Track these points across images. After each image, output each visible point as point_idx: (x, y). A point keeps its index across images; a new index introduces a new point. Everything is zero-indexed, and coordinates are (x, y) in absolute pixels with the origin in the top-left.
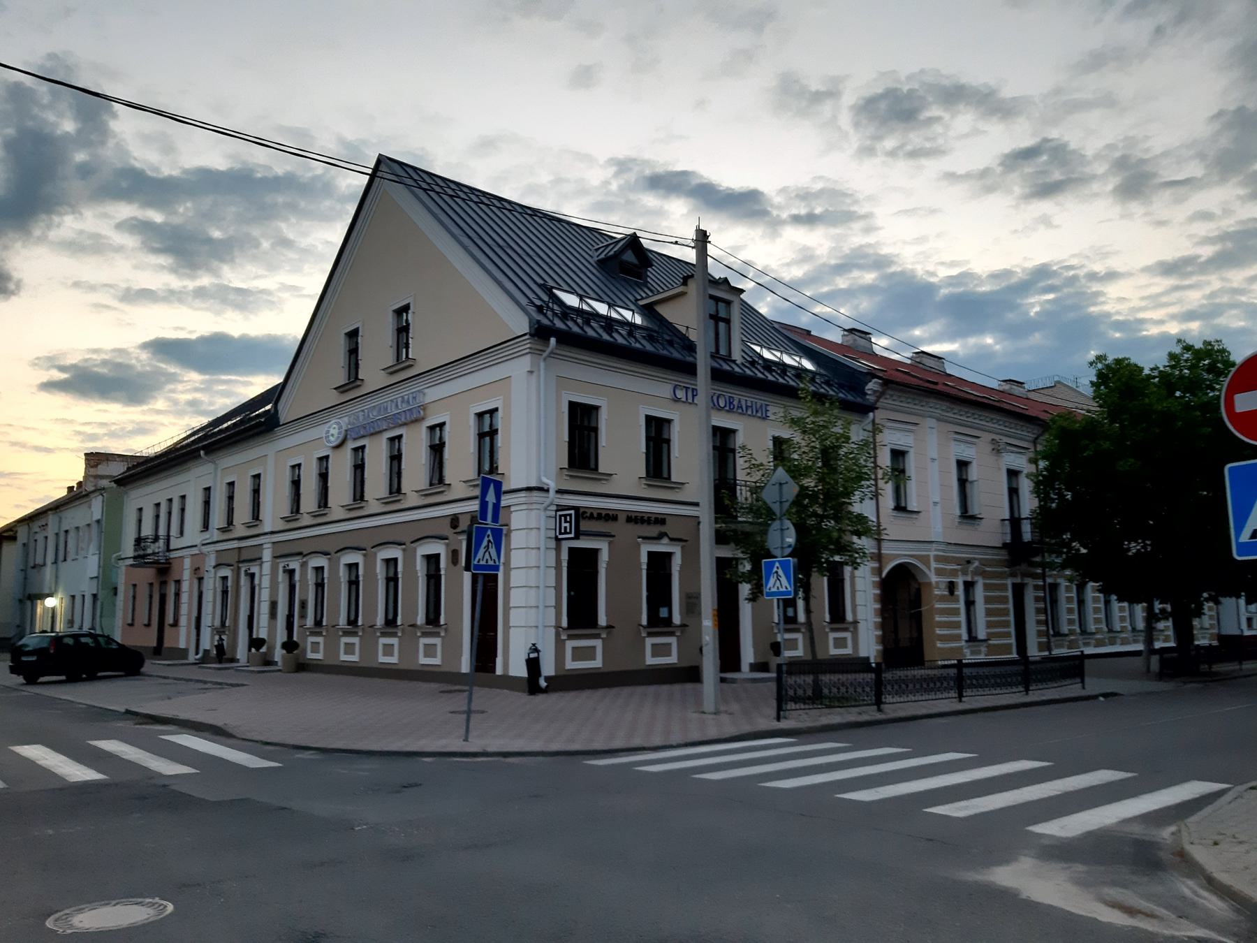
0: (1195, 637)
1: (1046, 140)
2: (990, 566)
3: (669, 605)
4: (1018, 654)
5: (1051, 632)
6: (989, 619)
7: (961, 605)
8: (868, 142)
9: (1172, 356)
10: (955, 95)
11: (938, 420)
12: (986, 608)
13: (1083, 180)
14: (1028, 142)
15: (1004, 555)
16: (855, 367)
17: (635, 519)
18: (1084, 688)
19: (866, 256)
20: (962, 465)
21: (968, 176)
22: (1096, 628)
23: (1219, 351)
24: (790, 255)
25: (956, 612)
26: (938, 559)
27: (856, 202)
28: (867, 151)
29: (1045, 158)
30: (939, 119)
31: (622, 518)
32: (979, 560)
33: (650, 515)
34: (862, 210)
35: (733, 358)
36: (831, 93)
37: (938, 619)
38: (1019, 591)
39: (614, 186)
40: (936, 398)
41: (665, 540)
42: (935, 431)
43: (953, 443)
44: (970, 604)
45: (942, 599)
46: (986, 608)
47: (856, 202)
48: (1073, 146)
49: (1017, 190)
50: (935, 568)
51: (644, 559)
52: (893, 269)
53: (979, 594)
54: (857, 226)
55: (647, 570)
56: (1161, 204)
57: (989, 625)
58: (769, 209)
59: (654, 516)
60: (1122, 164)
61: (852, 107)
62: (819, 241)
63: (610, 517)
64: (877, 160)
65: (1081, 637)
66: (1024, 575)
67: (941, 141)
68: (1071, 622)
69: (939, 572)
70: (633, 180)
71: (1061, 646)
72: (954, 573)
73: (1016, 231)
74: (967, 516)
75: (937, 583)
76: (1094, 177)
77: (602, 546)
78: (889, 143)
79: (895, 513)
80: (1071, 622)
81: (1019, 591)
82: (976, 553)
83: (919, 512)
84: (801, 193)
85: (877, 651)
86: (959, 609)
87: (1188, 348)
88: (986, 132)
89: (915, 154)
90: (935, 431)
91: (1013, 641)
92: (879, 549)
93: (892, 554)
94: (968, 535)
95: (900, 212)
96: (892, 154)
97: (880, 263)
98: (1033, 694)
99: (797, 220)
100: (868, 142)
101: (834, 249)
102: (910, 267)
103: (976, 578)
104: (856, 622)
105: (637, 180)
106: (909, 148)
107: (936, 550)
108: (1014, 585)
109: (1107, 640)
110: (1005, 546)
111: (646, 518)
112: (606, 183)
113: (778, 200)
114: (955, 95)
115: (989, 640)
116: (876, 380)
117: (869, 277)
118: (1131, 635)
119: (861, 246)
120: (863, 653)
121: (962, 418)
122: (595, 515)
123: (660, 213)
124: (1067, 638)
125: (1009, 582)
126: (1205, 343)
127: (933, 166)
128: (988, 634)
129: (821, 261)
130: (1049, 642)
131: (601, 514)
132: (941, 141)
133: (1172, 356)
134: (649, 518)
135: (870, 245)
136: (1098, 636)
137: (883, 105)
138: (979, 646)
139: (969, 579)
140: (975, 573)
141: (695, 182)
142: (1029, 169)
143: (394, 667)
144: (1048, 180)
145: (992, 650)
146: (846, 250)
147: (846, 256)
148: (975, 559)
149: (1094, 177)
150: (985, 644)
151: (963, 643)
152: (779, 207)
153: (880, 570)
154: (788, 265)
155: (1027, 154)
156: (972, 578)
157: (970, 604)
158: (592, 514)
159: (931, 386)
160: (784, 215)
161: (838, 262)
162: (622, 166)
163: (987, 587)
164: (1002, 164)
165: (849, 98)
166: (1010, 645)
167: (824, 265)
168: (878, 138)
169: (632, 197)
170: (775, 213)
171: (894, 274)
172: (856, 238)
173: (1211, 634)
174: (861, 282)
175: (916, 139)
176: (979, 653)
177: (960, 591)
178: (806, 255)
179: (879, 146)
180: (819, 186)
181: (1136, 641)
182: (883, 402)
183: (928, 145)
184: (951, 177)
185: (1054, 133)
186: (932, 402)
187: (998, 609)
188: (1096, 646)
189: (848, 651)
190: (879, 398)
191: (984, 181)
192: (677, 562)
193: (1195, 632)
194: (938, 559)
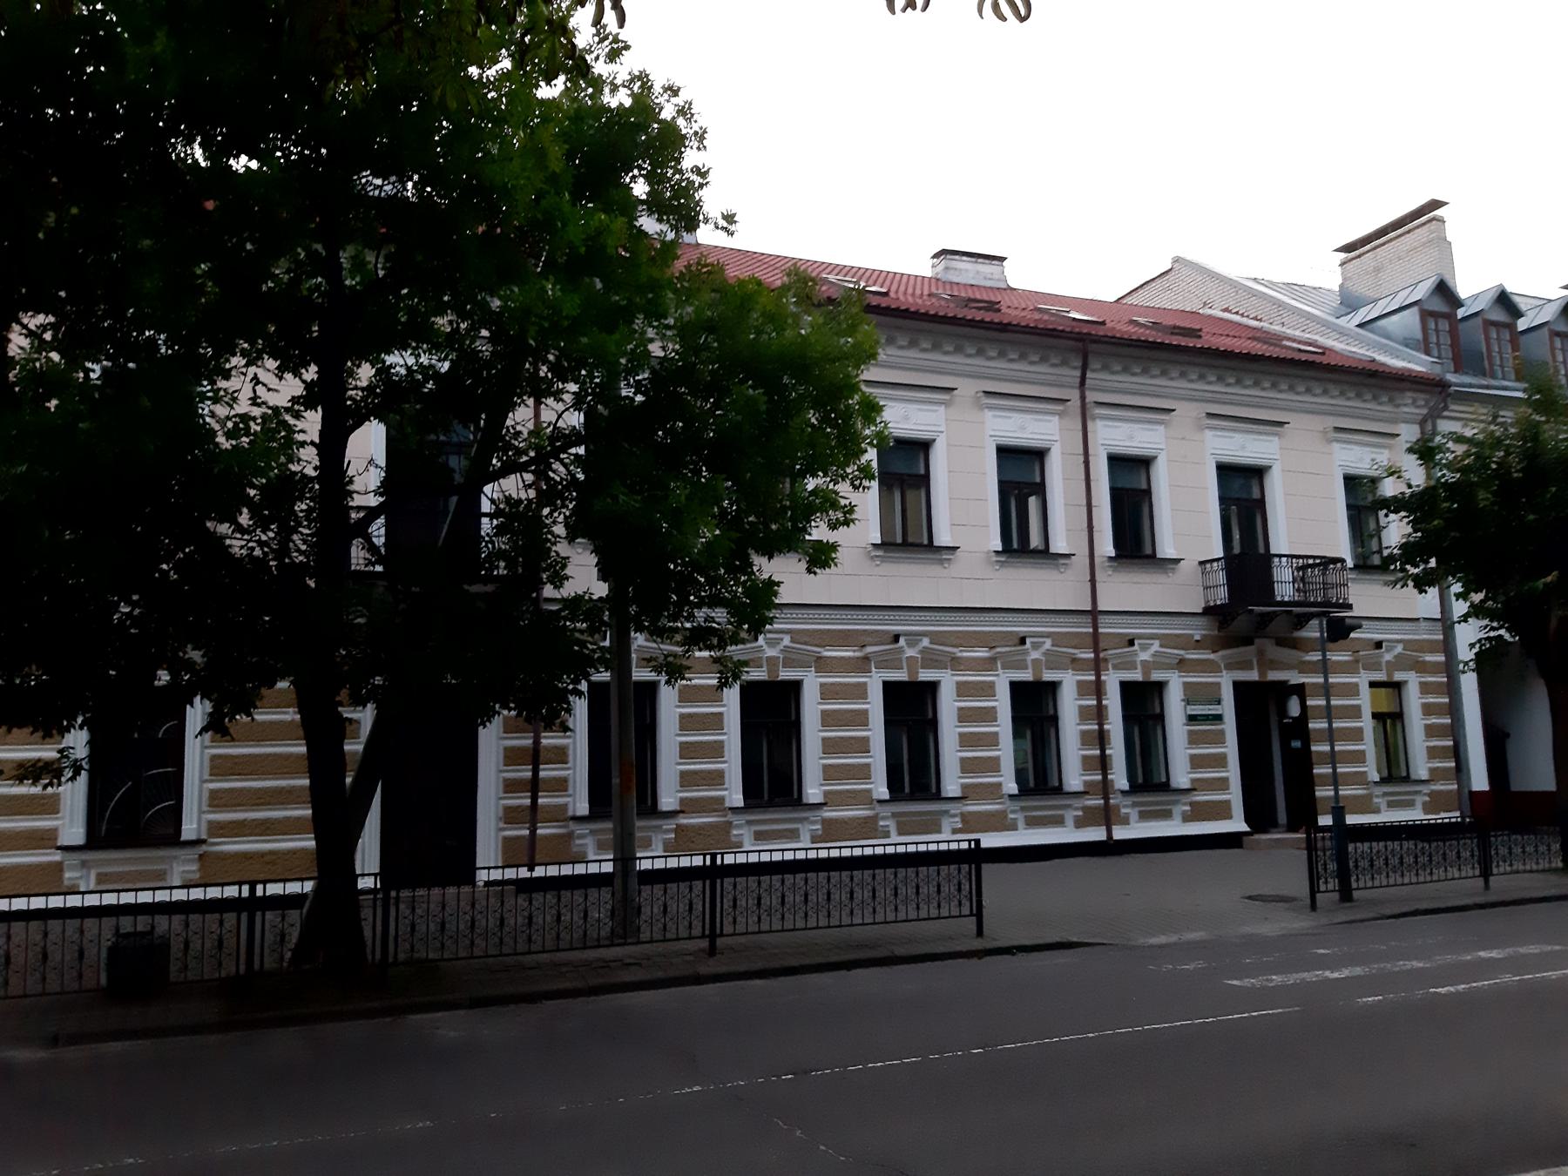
4: (1247, 821)
57: (218, 800)
110: (1209, 611)
124: (670, 824)
125: (1002, 681)
128: (1432, 771)
140: (1401, 663)
145: (832, 831)
148: (924, 634)
150: (192, 853)
188: (1187, 818)
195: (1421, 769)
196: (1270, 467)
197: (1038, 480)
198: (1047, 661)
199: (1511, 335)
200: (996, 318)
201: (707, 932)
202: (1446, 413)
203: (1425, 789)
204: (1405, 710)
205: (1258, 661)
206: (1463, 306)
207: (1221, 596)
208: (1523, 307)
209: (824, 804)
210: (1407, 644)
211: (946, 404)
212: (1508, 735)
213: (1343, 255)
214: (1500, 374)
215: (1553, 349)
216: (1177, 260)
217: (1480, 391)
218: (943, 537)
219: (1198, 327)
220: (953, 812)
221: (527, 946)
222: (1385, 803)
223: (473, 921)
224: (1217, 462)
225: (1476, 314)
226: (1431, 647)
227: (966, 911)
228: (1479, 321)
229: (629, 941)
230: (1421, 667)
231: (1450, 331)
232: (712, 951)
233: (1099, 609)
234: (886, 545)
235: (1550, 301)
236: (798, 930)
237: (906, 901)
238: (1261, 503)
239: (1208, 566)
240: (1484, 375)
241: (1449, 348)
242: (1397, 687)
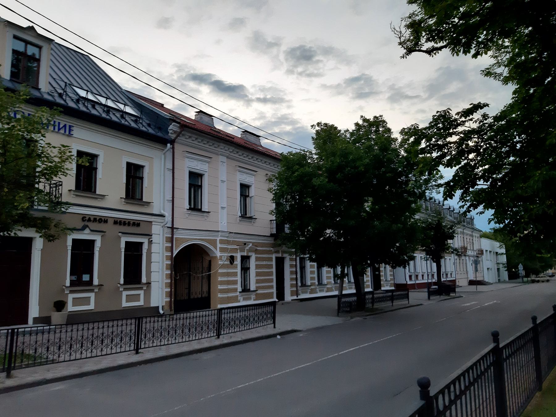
0: (382, 285)
1: (363, 74)
2: (262, 247)
3: (90, 272)
4: (277, 298)
5: (299, 284)
6: (271, 277)
7: (239, 270)
8: (291, 68)
9: (357, 124)
10: (328, 51)
11: (228, 157)
12: (256, 272)
13: (377, 93)
14: (356, 75)
15: (271, 241)
16: (163, 115)
17: (118, 222)
18: (275, 327)
19: (287, 119)
20: (244, 187)
21: (331, 87)
22: (327, 282)
23: (381, 121)
24: (255, 115)
25: (235, 274)
26: (222, 242)
27: (285, 94)
28: (290, 72)
29: (362, 82)
30: (321, 61)
31: (111, 222)
32: (253, 243)
33: (130, 221)
34: (287, 98)
35: (39, 88)
36: (275, 44)
37: (220, 279)
38: (280, 262)
39: (175, 77)
40: (224, 143)
41: (87, 231)
42: (225, 164)
43: (238, 173)
44: (245, 269)
45: (223, 266)
46: (256, 272)
47: (285, 94)
48: (374, 78)
49: (351, 95)
50: (220, 248)
51: (123, 245)
52: (299, 125)
53: (253, 263)
54: (284, 105)
55: (72, 250)
56: (405, 104)
57: (258, 281)
58: (248, 94)
59: (123, 220)
60: (392, 87)
61: (284, 52)
62: (268, 110)
63: (103, 220)
64: (295, 76)
65: (318, 287)
66: (283, 252)
67: (321, 71)
68: (312, 278)
69: (222, 250)
70: (184, 75)
71: (306, 292)
72: (235, 250)
73: (349, 112)
74: (245, 216)
75: (220, 256)
76: (381, 92)
77: (98, 238)
78: (300, 69)
79: (190, 212)
80: (312, 278)
81: (280, 262)
82: (251, 239)
83: (209, 212)
84: (261, 88)
85: (166, 302)
86: (237, 272)
87: (365, 120)
88: (340, 68)
89: (309, 75)
90: (225, 164)
91: (274, 290)
92: (173, 234)
93: (185, 238)
94: (245, 228)
95: (303, 100)
96: (300, 74)
97: (293, 122)
98: (223, 338)
99: (259, 100)
100: (291, 68)
101: (274, 114)
102: (305, 125)
103: (285, 255)
104: (149, 284)
105: (186, 76)
106: (308, 72)
107: (221, 236)
108: (277, 258)
109: (333, 288)
110: (272, 235)
111: (127, 222)
112: (172, 75)
113: (252, 90)
114: (328, 51)
115: (257, 291)
116: (174, 123)
117: (288, 128)
118: (348, 285)
119: (285, 114)
120: (153, 304)
121: (244, 159)
122: (92, 219)
123: (198, 91)
124: (310, 288)
125: (274, 256)
126: (375, 117)
127: (317, 81)
128: (257, 287)
129: (268, 119)
130: (297, 291)
131: (96, 218)
132: (321, 71)
133: (357, 124)
134: (124, 222)
135: (289, 114)
136: (328, 286)
137: (298, 53)
138: (250, 295)
139: (245, 254)
140: (250, 250)
141: (213, 79)
142: (355, 86)
143: (92, 311)
144: (363, 92)
145: (258, 297)
146: (279, 115)
147: (279, 118)
148: (250, 242)
149: (381, 92)
150: (254, 293)
151: (238, 293)
152: (252, 94)
153: (171, 249)
154: (254, 119)
155: (355, 80)
156: (282, 255)
157: (245, 269)
158: (90, 218)
159: (231, 139)
160: (254, 98)
161: (275, 120)
162: (180, 68)
163: (257, 259)
164: (345, 83)
165: (284, 48)
166: (273, 293)
167: (269, 121)
168: (295, 66)
169: (186, 83)
170: (250, 96)
171: (299, 128)
172: (283, 110)
173: (391, 283)
174: (285, 130)
175: (311, 69)
176: (250, 299)
177: (238, 262)
178: (262, 116)
179: (295, 70)
180: (269, 85)
181: (350, 288)
182: (181, 139)
183: (316, 72)
184: (324, 87)
185: (367, 72)
186: (222, 145)
187: (264, 272)
188: (311, 293)
189: (141, 303)
190: (178, 136)
191: (338, 90)
192: (145, 247)
193: (382, 283)
194: (222, 242)
196: (251, 186)
197: (200, 184)
204: (306, 265)
207: (274, 231)
210: (253, 244)
211: (208, 162)
218: (205, 208)
221: (101, 353)
222: (242, 298)
223: (59, 349)
224: (240, 183)
229: (390, 294)
232: (392, 305)
233: (174, 227)
234: (190, 209)
238: (201, 186)
239: (273, 222)
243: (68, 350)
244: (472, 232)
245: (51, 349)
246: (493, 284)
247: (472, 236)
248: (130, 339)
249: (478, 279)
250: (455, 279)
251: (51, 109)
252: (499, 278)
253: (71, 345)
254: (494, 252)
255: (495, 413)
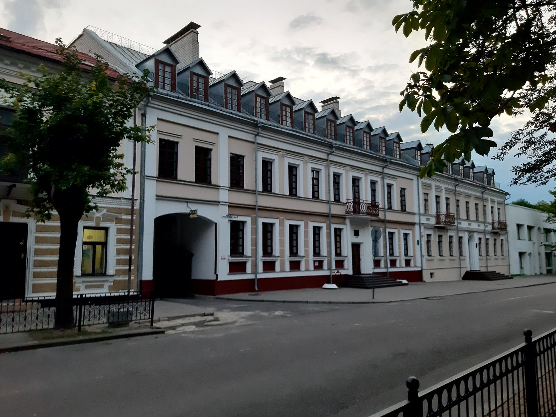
128: (117, 271)
140: (106, 218)
195: (111, 269)
198: (103, 218)
199: (353, 131)
200: (8, 44)
201: (150, 317)
202: (149, 104)
203: (111, 279)
205: (4, 211)
206: (373, 131)
208: (297, 102)
209: (115, 275)
212: (192, 255)
213: (322, 104)
214: (348, 143)
215: (327, 125)
216: (85, 30)
217: (162, 96)
219: (10, 37)
220: (110, 280)
225: (344, 123)
226: (126, 212)
227: (147, 317)
228: (188, 73)
230: (119, 221)
231: (265, 104)
235: (257, 84)
236: (8, 333)
237: (94, 317)
240: (393, 156)
241: (237, 101)
242: (106, 229)
243: (46, 319)
244: (482, 193)
245: (34, 318)
246: (515, 278)
247: (483, 200)
248: (145, 310)
249: (490, 269)
250: (420, 269)
251: (531, 111)
252: (549, 268)
253: (100, 311)
254: (539, 229)
255: (540, 380)
